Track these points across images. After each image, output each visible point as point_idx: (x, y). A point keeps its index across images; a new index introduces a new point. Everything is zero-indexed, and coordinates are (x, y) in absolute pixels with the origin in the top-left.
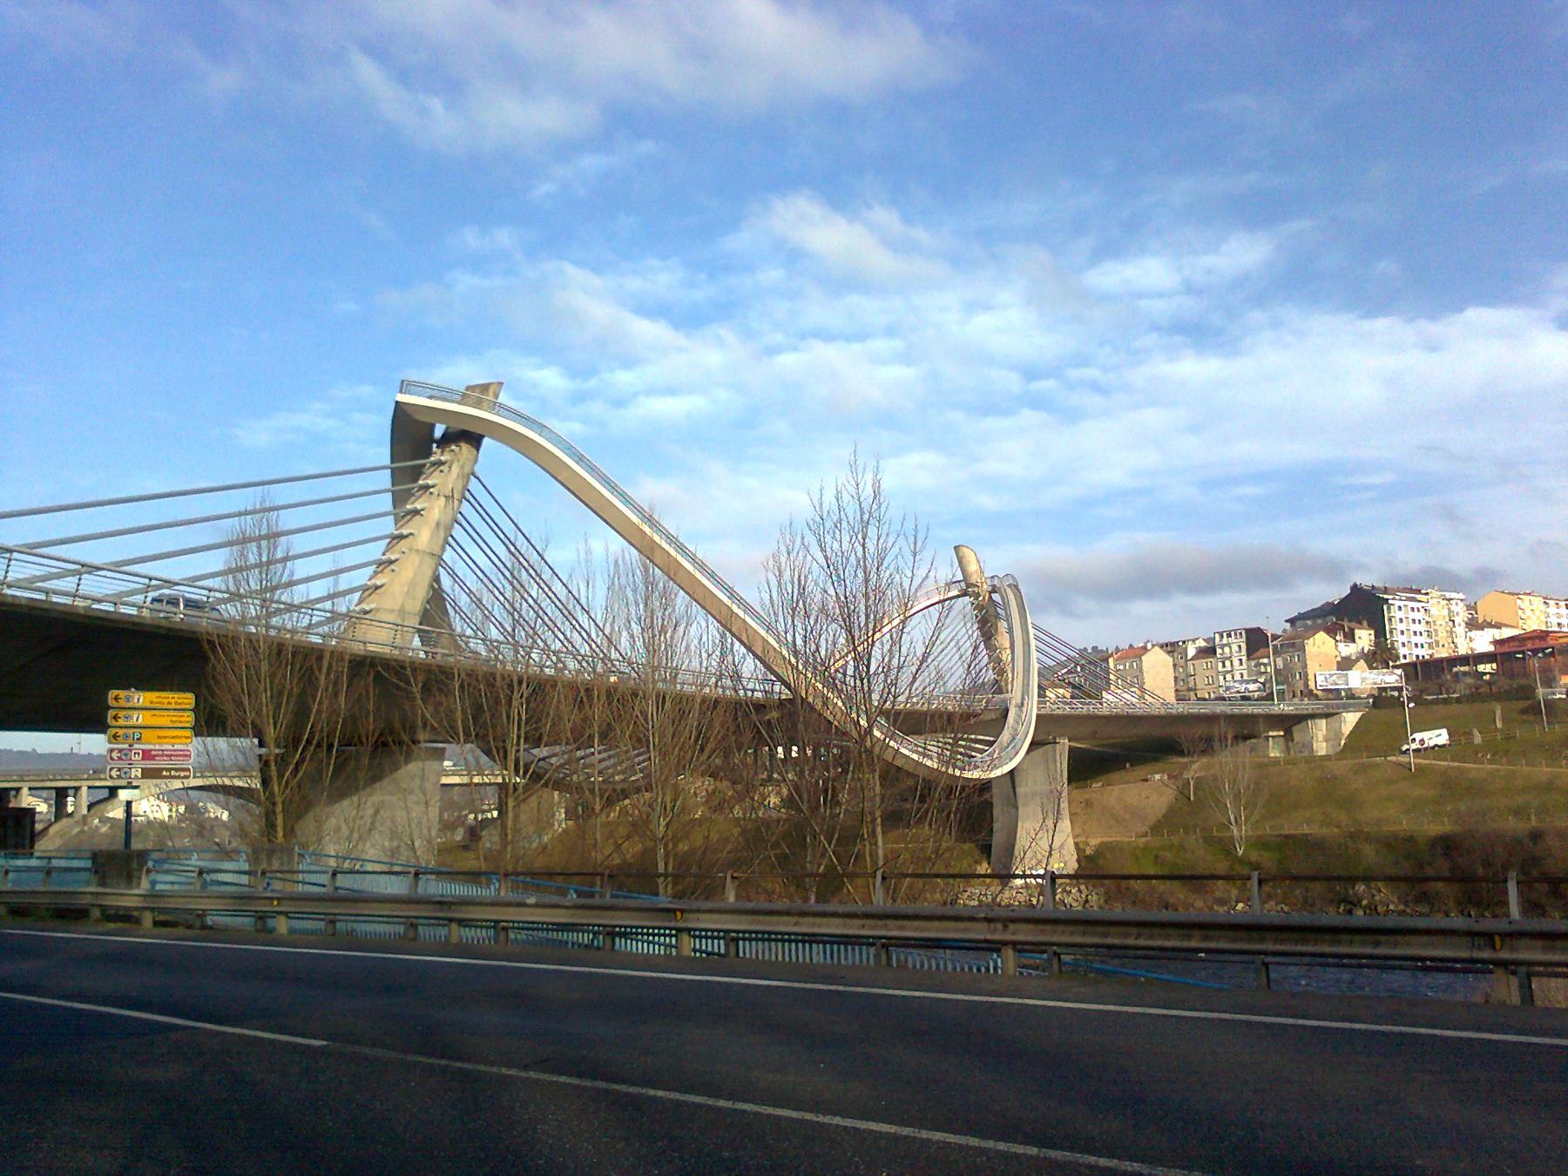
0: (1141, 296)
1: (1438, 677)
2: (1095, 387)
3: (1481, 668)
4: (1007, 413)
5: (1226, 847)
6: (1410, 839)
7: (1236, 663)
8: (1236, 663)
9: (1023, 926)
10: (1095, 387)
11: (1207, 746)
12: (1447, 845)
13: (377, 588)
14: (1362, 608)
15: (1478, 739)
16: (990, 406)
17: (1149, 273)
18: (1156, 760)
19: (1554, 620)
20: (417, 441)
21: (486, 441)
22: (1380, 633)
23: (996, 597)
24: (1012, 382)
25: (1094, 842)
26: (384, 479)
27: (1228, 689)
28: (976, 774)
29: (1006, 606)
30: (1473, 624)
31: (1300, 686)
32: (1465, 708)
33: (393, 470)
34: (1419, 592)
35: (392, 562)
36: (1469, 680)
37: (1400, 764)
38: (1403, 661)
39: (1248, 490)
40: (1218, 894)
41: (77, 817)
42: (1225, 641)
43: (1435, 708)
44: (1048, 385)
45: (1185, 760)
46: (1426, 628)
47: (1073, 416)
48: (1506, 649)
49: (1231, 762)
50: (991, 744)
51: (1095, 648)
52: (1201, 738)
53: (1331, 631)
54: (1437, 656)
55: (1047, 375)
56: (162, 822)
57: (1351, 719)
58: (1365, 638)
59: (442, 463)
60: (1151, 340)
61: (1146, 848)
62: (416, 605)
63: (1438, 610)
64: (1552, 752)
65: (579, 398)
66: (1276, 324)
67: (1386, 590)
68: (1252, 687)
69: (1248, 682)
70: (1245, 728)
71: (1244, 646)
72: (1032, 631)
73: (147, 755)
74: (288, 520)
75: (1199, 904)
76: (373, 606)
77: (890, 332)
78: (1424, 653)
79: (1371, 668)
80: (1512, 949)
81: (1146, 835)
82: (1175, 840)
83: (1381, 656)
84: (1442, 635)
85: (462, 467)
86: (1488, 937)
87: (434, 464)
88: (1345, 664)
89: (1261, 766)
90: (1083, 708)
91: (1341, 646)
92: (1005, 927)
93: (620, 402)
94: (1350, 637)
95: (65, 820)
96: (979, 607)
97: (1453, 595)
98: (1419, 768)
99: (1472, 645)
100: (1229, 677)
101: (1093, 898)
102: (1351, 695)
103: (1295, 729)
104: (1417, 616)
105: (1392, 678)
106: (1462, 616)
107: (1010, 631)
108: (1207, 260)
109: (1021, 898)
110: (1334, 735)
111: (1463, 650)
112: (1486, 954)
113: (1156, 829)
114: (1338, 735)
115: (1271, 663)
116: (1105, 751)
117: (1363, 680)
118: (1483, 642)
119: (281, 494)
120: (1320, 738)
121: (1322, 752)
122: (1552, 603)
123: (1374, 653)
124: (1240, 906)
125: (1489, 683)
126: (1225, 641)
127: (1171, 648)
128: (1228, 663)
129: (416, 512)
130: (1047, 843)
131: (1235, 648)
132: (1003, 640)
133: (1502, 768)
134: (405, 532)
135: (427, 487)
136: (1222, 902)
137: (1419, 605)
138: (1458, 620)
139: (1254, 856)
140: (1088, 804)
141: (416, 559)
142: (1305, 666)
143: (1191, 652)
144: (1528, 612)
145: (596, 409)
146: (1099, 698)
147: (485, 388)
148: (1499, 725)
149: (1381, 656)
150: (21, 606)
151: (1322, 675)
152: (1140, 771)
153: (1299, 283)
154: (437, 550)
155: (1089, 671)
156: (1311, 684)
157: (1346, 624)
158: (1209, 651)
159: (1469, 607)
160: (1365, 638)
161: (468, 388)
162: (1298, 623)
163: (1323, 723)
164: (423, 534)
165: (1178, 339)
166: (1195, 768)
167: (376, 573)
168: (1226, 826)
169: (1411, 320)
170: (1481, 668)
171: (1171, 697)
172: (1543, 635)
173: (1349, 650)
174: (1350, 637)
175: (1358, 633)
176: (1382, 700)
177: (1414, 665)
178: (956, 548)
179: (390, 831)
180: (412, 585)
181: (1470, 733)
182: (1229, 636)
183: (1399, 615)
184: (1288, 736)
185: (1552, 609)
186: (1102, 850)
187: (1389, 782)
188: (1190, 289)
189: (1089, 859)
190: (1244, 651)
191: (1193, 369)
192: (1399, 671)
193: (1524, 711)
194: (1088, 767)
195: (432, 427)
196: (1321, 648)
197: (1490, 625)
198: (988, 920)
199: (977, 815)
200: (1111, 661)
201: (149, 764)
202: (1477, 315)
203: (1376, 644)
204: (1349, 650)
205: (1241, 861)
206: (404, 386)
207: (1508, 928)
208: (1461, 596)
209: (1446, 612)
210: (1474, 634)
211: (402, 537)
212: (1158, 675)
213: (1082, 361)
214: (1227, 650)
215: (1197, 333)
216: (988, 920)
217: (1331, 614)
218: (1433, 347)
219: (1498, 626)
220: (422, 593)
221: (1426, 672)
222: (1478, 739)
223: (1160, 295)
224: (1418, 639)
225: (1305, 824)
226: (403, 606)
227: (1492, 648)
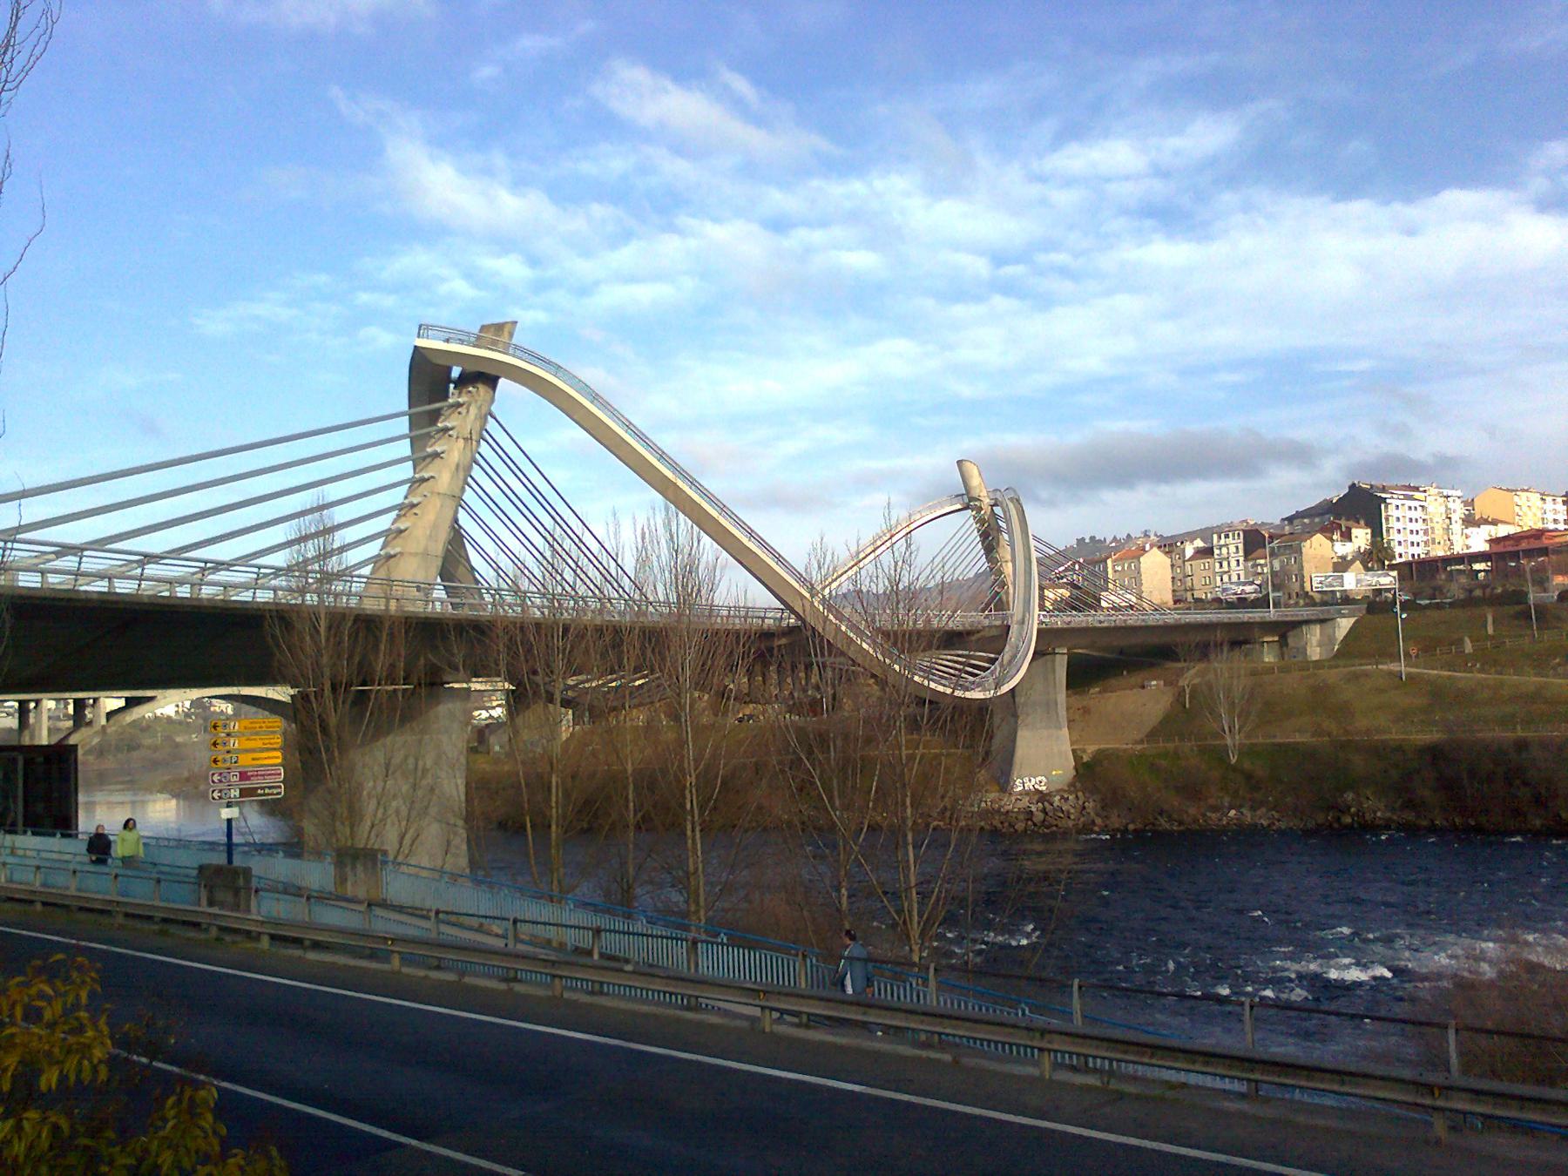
0: (1108, 180)
1: (1433, 577)
2: (1064, 272)
3: (1477, 566)
4: (978, 299)
5: (1220, 755)
6: (1399, 749)
7: (1234, 563)
8: (1234, 563)
9: (1056, 1037)
10: (1064, 272)
11: (1204, 651)
12: (1434, 754)
13: (401, 531)
14: (1360, 505)
15: (1468, 647)
16: (959, 291)
17: (1116, 155)
18: (1152, 665)
19: (1550, 516)
20: (436, 383)
21: (502, 382)
22: (1377, 532)
23: (998, 510)
24: (980, 267)
25: (1092, 749)
26: (402, 425)
27: (1224, 590)
28: (977, 694)
29: (1008, 521)
30: (1470, 521)
31: (1296, 587)
32: (1458, 612)
33: (411, 416)
34: (1417, 489)
35: (413, 506)
36: (1463, 580)
37: (1390, 673)
38: (1398, 560)
40: (1211, 801)
41: (96, 727)
42: (1222, 542)
43: (1428, 612)
45: (1179, 665)
46: (1423, 527)
47: (1045, 302)
48: (1499, 548)
49: (1225, 671)
50: (992, 661)
51: (1092, 538)
52: (1197, 645)
53: (1328, 531)
54: (1432, 554)
55: (1017, 261)
56: (169, 718)
57: (1344, 625)
58: (1361, 537)
59: (459, 405)
61: (1141, 755)
62: (439, 548)
63: (1436, 507)
64: (1540, 662)
65: (540, 287)
66: (1247, 207)
68: (1248, 589)
69: (1245, 584)
70: (1240, 638)
71: (1241, 546)
72: (1033, 543)
73: (244, 776)
74: (340, 514)
75: (1192, 811)
76: (398, 550)
78: (1420, 551)
79: (1367, 569)
80: (1447, 1099)
81: (1141, 742)
82: (1170, 746)
83: (1377, 556)
84: (1439, 534)
85: (480, 408)
86: (1429, 1088)
87: (452, 406)
88: (1342, 565)
89: (1254, 673)
90: (1079, 619)
91: (1338, 545)
92: (1042, 1035)
93: (584, 290)
94: (1347, 536)
95: (83, 730)
96: (981, 521)
97: (1450, 493)
98: (1409, 675)
99: (1468, 542)
100: (1226, 578)
101: (1090, 805)
102: (1347, 599)
103: (1290, 634)
104: (1413, 514)
105: (1388, 580)
106: (1459, 511)
107: (1012, 544)
108: (1174, 142)
109: (1021, 805)
110: (1328, 640)
111: (1458, 549)
112: (1428, 1101)
113: (1152, 735)
114: (1332, 639)
115: (1265, 565)
116: (1102, 659)
117: (1358, 581)
118: (1478, 541)
119: (334, 492)
120: (1314, 644)
121: (1315, 657)
122: (1549, 499)
123: (1370, 553)
124: (1232, 813)
125: (1484, 587)
126: (1222, 542)
127: (1169, 545)
128: (1225, 564)
129: (436, 455)
130: (1042, 764)
132: (1004, 552)
133: (1491, 677)
134: (426, 475)
135: (446, 430)
136: (1214, 809)
137: (1417, 504)
138: (1455, 517)
139: (1247, 765)
140: (1086, 711)
141: (437, 502)
142: (1301, 568)
144: (1525, 509)
145: (560, 297)
146: (1096, 606)
147: (499, 328)
148: (1490, 630)
149: (1377, 556)
150: (89, 600)
151: (1317, 578)
152: (1136, 679)
153: (1268, 164)
154: (457, 492)
155: (1087, 566)
156: (1308, 588)
157: (1343, 523)
158: (1207, 552)
159: (1466, 503)
160: (1361, 537)
161: (483, 328)
162: (1296, 522)
163: (1317, 629)
164: (443, 476)
165: (1149, 223)
166: (1191, 675)
167: (399, 516)
168: (1219, 735)
169: (1387, 203)
170: (1477, 566)
171: (1168, 598)
172: (1539, 534)
173: (1344, 549)
174: (1347, 536)
175: (1355, 532)
176: (1376, 604)
177: (1408, 564)
178: (959, 462)
179: (422, 778)
180: (435, 526)
181: (1460, 642)
182: (1227, 536)
183: (1396, 513)
185: (1549, 505)
186: (1100, 757)
187: (1380, 691)
188: (1161, 172)
189: (1087, 765)
190: (1241, 553)
191: (1166, 254)
192: (1395, 573)
193: (1516, 616)
194: (1083, 674)
195: (449, 369)
196: (1319, 549)
197: (1486, 522)
198: (1028, 1029)
199: (981, 732)
200: (1109, 562)
201: (247, 784)
202: (1457, 199)
203: (1373, 544)
204: (1344, 549)
205: (1234, 769)
206: (423, 329)
207: (1446, 1083)
208: (1459, 493)
209: (1443, 509)
210: (1469, 531)
211: (423, 480)
212: (1156, 573)
213: (1050, 245)
215: (1167, 216)
216: (1028, 1029)
218: (1411, 232)
219: (1495, 523)
220: (444, 535)
221: (1421, 572)
222: (1468, 647)
223: (1127, 178)
224: (1415, 538)
225: (1297, 733)
226: (426, 549)
227: (1485, 547)
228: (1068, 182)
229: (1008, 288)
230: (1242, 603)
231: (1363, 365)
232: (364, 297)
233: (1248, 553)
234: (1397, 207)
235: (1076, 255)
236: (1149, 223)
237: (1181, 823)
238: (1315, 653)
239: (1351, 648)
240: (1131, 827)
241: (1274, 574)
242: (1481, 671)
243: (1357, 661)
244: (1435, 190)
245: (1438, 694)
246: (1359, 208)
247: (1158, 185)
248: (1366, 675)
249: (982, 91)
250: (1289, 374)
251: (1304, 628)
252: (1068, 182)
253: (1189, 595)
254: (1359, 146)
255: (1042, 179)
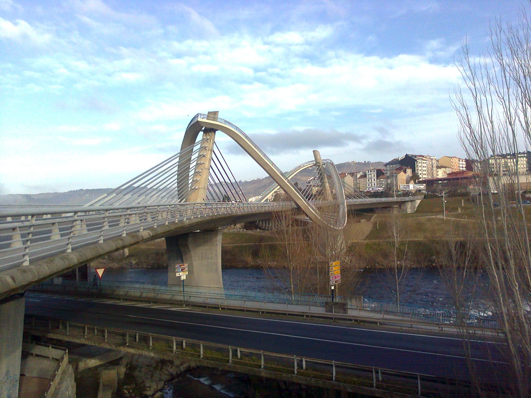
0: (291, 45)
1: (432, 185)
2: (279, 75)
4: (250, 83)
7: (373, 180)
8: (373, 180)
10: (279, 75)
14: (409, 162)
16: (243, 81)
17: (294, 37)
22: (414, 171)
24: (250, 73)
37: (440, 219)
38: (421, 180)
39: (335, 113)
44: (263, 74)
47: (272, 85)
48: (451, 177)
55: (262, 71)
58: (409, 171)
60: (296, 60)
66: (337, 57)
67: (416, 156)
68: (380, 189)
71: (375, 175)
77: (205, 53)
101: (353, 260)
110: (413, 207)
113: (368, 237)
114: (414, 207)
120: (409, 209)
121: (409, 212)
127: (352, 174)
128: (370, 180)
131: (373, 175)
138: (434, 165)
142: (397, 183)
143: (358, 176)
149: (415, 177)
153: (342, 42)
158: (364, 176)
165: (305, 60)
169: (382, 58)
175: (407, 170)
182: (371, 171)
183: (420, 165)
184: (400, 205)
187: (438, 224)
191: (311, 70)
202: (404, 58)
213: (272, 66)
214: (370, 176)
215: (312, 57)
217: (396, 164)
218: (391, 68)
219: (445, 167)
221: (430, 183)
223: (297, 45)
228: (277, 45)
229: (260, 80)
230: (376, 195)
231: (379, 111)
232: (28, 73)
233: (378, 177)
234: (386, 60)
235: (283, 70)
236: (305, 60)
237: (383, 266)
238: (409, 211)
239: (420, 210)
240: (367, 267)
241: (388, 184)
242: (468, 218)
243: (430, 214)
244: (398, 54)
245: (457, 226)
246: (374, 59)
247: (307, 48)
248: (433, 219)
249: (245, 13)
250: (355, 113)
251: (407, 203)
252: (277, 45)
253: (358, 190)
254: (371, 38)
255: (266, 43)
